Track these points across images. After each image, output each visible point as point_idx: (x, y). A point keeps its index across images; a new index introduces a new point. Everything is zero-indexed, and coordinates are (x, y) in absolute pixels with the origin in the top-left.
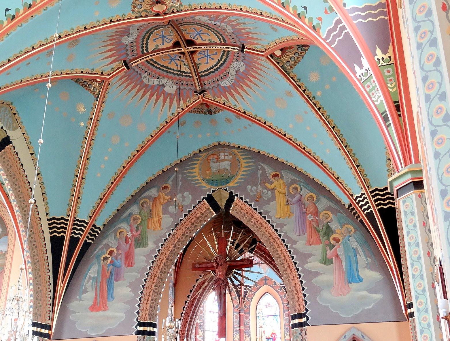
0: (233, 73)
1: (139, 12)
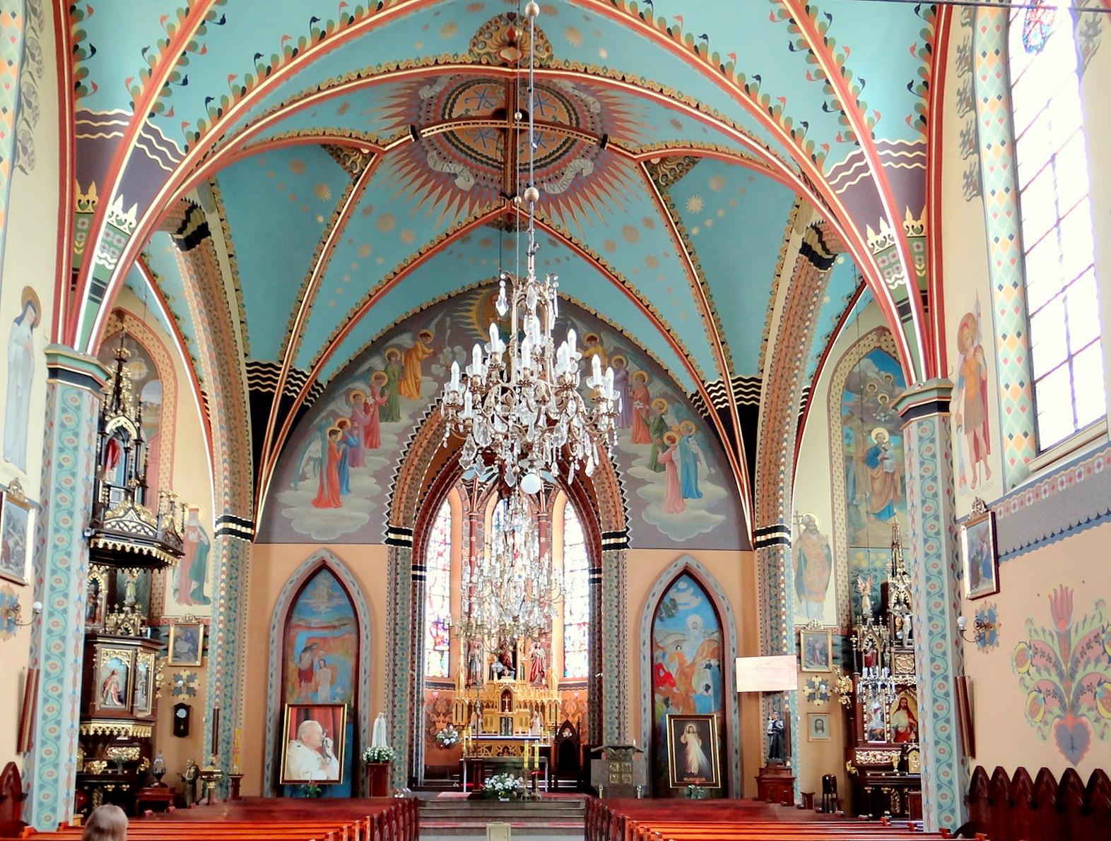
0: (569, 175)
1: (479, 54)
